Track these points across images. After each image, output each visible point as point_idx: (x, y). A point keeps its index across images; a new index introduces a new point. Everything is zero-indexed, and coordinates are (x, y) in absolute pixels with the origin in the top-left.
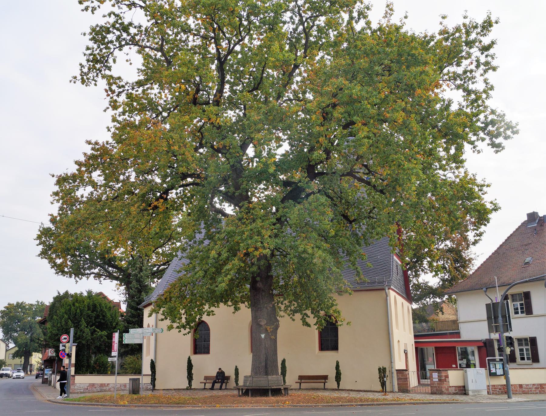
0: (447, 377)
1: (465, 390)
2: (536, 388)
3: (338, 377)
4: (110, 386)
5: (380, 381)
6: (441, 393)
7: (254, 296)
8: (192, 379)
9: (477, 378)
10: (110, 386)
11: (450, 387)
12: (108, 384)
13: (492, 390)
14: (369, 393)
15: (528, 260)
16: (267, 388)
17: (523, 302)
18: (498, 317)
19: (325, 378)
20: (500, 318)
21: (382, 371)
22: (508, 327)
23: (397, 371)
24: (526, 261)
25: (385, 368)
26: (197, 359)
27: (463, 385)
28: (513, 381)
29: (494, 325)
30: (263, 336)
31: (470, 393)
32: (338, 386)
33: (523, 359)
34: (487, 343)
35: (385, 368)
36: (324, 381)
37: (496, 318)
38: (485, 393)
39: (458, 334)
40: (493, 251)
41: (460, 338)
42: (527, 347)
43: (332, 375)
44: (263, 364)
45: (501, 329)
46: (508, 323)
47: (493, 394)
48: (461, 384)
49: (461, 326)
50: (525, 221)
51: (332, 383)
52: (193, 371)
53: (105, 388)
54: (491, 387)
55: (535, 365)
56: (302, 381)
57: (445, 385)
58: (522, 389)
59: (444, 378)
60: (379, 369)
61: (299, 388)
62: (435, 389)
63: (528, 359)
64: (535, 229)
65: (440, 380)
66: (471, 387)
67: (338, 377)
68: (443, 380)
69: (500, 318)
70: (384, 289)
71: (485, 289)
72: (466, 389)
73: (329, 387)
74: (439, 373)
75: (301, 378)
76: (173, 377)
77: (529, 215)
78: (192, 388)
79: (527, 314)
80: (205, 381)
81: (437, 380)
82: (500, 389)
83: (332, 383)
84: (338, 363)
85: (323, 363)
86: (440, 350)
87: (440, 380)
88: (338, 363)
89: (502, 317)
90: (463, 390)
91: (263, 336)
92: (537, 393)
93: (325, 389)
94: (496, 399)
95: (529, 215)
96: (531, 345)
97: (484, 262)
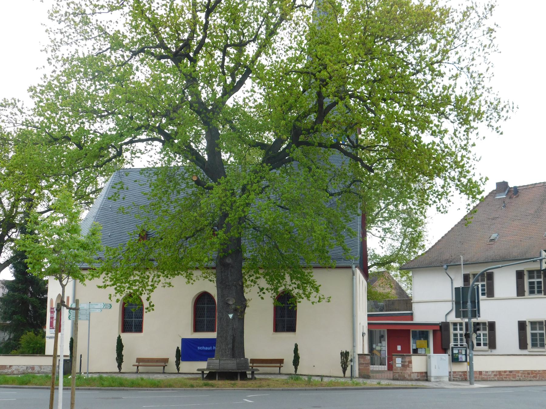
0: (410, 362)
1: (427, 377)
2: (495, 375)
3: (296, 361)
4: (13, 369)
5: (342, 366)
6: (404, 379)
7: (222, 272)
8: (122, 362)
9: (439, 364)
10: (13, 369)
11: (413, 373)
12: (10, 366)
13: (453, 377)
14: (338, 379)
15: (494, 236)
16: (237, 371)
17: (485, 283)
18: (467, 302)
19: (281, 361)
20: (469, 304)
21: (345, 355)
22: (476, 313)
23: (359, 355)
24: (492, 238)
25: (348, 353)
26: (127, 337)
27: (425, 371)
28: (476, 368)
29: (462, 309)
30: (231, 316)
31: (432, 379)
32: (296, 371)
33: (479, 344)
34: (443, 327)
35: (348, 353)
36: (279, 365)
37: (465, 303)
38: (447, 379)
39: (411, 316)
40: (456, 223)
41: (412, 320)
42: (485, 332)
43: (289, 359)
44: (230, 346)
45: (470, 314)
46: (477, 309)
47: (454, 380)
48: (423, 370)
49: (414, 306)
50: (494, 191)
51: (288, 367)
52: (123, 353)
53: (6, 371)
54: (452, 373)
55: (494, 352)
56: (140, 364)
57: (408, 371)
58: (482, 377)
59: (407, 364)
60: (342, 354)
61: (162, 371)
62: (397, 375)
63: (485, 344)
64: (503, 201)
65: (403, 366)
66: (434, 373)
67: (296, 361)
68: (406, 365)
69: (469, 304)
70: (350, 267)
71: (445, 267)
72: (428, 374)
73: (167, 372)
74: (402, 359)
75: (139, 360)
76: (99, 358)
77: (498, 184)
78: (180, 372)
79: (488, 297)
80: (137, 364)
81: (400, 365)
82: (461, 376)
83: (288, 367)
84: (296, 346)
85: (279, 346)
86: (396, 333)
87: (403, 366)
88: (296, 346)
89: (471, 302)
90: (425, 376)
91: (231, 316)
92: (495, 380)
93: (280, 374)
94: (459, 385)
95: (498, 184)
96: (490, 330)
97: (446, 235)
